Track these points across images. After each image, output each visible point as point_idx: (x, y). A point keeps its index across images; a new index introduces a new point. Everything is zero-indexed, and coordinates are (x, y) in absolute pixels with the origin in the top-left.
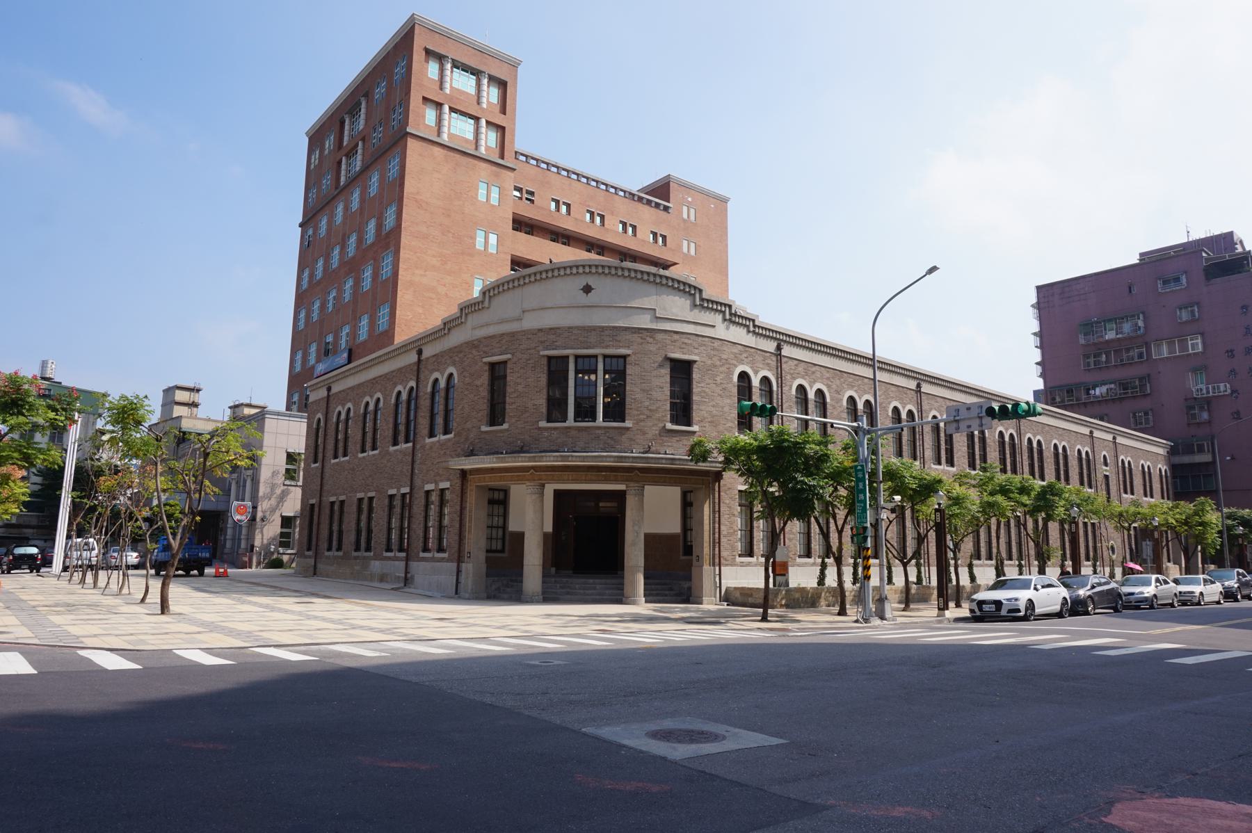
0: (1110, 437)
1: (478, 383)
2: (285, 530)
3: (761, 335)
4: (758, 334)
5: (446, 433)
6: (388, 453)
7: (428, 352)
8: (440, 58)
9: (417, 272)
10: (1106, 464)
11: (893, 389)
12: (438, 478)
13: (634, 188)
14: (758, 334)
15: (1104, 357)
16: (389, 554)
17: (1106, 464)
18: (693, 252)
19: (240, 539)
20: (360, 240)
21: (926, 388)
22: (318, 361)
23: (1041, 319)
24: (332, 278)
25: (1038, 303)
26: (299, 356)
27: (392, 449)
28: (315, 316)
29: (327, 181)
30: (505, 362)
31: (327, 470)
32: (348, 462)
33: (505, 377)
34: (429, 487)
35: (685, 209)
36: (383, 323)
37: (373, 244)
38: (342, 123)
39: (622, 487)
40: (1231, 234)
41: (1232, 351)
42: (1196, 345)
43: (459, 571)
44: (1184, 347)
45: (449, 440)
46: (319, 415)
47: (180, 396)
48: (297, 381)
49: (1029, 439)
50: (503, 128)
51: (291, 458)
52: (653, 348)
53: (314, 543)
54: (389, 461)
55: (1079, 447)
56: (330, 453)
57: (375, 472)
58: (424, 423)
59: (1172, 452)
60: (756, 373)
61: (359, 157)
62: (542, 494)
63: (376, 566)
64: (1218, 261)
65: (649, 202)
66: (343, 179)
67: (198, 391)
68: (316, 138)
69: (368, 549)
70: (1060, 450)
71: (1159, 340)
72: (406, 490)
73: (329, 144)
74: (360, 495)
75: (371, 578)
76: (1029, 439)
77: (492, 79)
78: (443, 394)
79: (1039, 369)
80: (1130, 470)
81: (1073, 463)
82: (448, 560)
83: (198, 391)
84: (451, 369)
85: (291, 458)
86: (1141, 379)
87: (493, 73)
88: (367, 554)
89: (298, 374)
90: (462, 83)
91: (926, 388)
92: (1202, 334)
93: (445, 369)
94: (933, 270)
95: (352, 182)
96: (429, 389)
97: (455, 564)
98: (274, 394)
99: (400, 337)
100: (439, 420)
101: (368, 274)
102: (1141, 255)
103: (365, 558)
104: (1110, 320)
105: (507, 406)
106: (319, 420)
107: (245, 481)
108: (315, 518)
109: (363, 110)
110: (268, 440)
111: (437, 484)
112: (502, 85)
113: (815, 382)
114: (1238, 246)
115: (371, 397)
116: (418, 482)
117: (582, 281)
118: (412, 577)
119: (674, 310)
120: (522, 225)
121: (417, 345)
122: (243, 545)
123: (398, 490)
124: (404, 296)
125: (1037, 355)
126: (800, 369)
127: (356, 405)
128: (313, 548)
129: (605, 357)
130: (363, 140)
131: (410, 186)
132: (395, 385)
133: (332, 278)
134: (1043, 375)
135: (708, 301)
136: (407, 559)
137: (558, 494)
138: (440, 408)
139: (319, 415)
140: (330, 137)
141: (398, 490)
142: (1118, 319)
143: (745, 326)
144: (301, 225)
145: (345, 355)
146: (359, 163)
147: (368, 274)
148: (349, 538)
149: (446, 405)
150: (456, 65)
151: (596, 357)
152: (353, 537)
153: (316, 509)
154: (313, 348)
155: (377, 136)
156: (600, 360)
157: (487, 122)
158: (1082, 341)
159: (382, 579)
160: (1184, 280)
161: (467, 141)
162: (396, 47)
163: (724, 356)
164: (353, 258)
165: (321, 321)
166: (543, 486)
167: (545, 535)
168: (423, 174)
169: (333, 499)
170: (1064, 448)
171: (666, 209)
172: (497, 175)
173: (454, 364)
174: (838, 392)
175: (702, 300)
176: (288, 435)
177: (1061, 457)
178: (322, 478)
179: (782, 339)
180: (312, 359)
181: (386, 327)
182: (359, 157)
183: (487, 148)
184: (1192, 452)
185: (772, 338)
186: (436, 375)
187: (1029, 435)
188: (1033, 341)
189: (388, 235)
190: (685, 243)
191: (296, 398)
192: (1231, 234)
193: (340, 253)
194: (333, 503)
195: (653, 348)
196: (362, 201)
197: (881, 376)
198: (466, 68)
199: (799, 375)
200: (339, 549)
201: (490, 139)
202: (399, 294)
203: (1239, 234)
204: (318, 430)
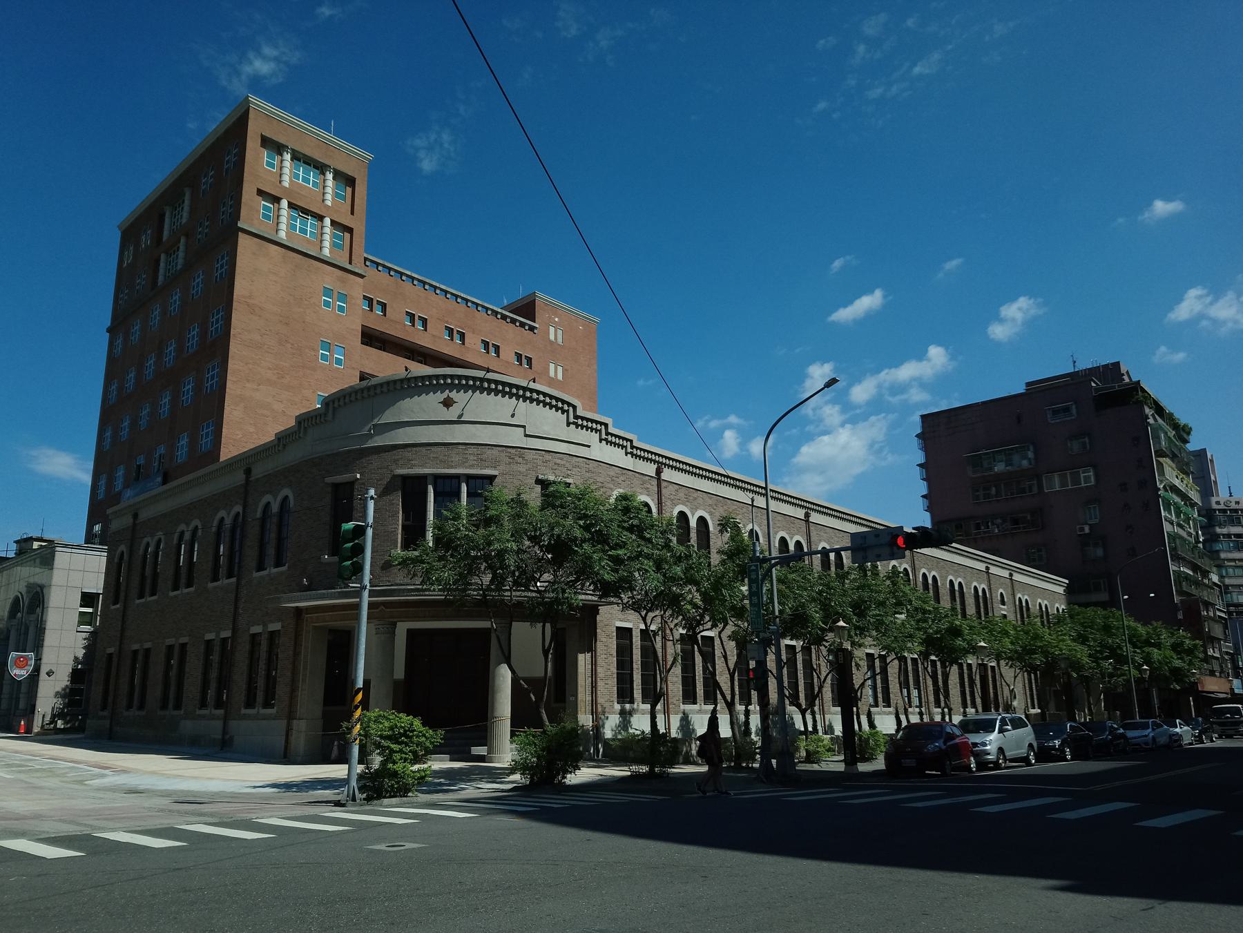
0: (1006, 574)
2: (77, 686)
3: (640, 457)
4: (636, 456)
5: (278, 565)
9: (247, 385)
10: (1003, 603)
14: (636, 456)
15: (993, 490)
17: (1003, 603)
18: (560, 377)
19: (18, 699)
21: (815, 518)
22: (126, 486)
23: (926, 448)
26: (103, 482)
27: (211, 585)
28: (125, 434)
34: (256, 629)
36: (205, 443)
38: (162, 216)
40: (1117, 365)
43: (289, 731)
44: (1076, 481)
48: (97, 511)
49: (924, 575)
52: (522, 468)
55: (975, 584)
58: (251, 554)
59: (1069, 590)
61: (181, 254)
62: (393, 634)
65: (513, 321)
66: (161, 278)
68: (129, 234)
72: (226, 634)
73: (146, 240)
74: (170, 641)
76: (924, 575)
78: (275, 520)
81: (970, 601)
82: (275, 718)
84: (286, 492)
85: (88, 599)
87: (340, 168)
88: (176, 713)
91: (815, 518)
92: (1095, 467)
96: (259, 514)
98: (70, 522)
99: (227, 452)
100: (271, 551)
102: (1028, 384)
107: (27, 628)
108: (114, 670)
109: (187, 202)
111: (265, 625)
113: (697, 509)
114: (1126, 377)
115: (188, 524)
117: (441, 396)
118: (231, 738)
119: (546, 428)
120: (371, 338)
121: (247, 461)
122: (22, 705)
123: (218, 634)
124: (232, 413)
125: (923, 488)
126: (681, 495)
130: (187, 236)
131: (241, 287)
134: (929, 509)
136: (226, 719)
137: (411, 633)
138: (272, 536)
139: (122, 548)
140: (144, 234)
141: (218, 634)
143: (623, 447)
144: (109, 330)
146: (180, 261)
148: (154, 693)
149: (279, 532)
151: (457, 477)
153: (115, 659)
154: (120, 473)
157: (333, 223)
162: (227, 132)
166: (395, 624)
167: (396, 683)
169: (135, 647)
170: (960, 584)
171: (532, 329)
175: (576, 417)
176: (81, 571)
178: (123, 622)
180: (119, 485)
182: (181, 254)
185: (651, 460)
186: (268, 498)
187: (923, 570)
190: (552, 366)
191: (97, 528)
192: (1117, 365)
194: (135, 652)
195: (522, 468)
197: (774, 506)
199: (680, 502)
200: (141, 707)
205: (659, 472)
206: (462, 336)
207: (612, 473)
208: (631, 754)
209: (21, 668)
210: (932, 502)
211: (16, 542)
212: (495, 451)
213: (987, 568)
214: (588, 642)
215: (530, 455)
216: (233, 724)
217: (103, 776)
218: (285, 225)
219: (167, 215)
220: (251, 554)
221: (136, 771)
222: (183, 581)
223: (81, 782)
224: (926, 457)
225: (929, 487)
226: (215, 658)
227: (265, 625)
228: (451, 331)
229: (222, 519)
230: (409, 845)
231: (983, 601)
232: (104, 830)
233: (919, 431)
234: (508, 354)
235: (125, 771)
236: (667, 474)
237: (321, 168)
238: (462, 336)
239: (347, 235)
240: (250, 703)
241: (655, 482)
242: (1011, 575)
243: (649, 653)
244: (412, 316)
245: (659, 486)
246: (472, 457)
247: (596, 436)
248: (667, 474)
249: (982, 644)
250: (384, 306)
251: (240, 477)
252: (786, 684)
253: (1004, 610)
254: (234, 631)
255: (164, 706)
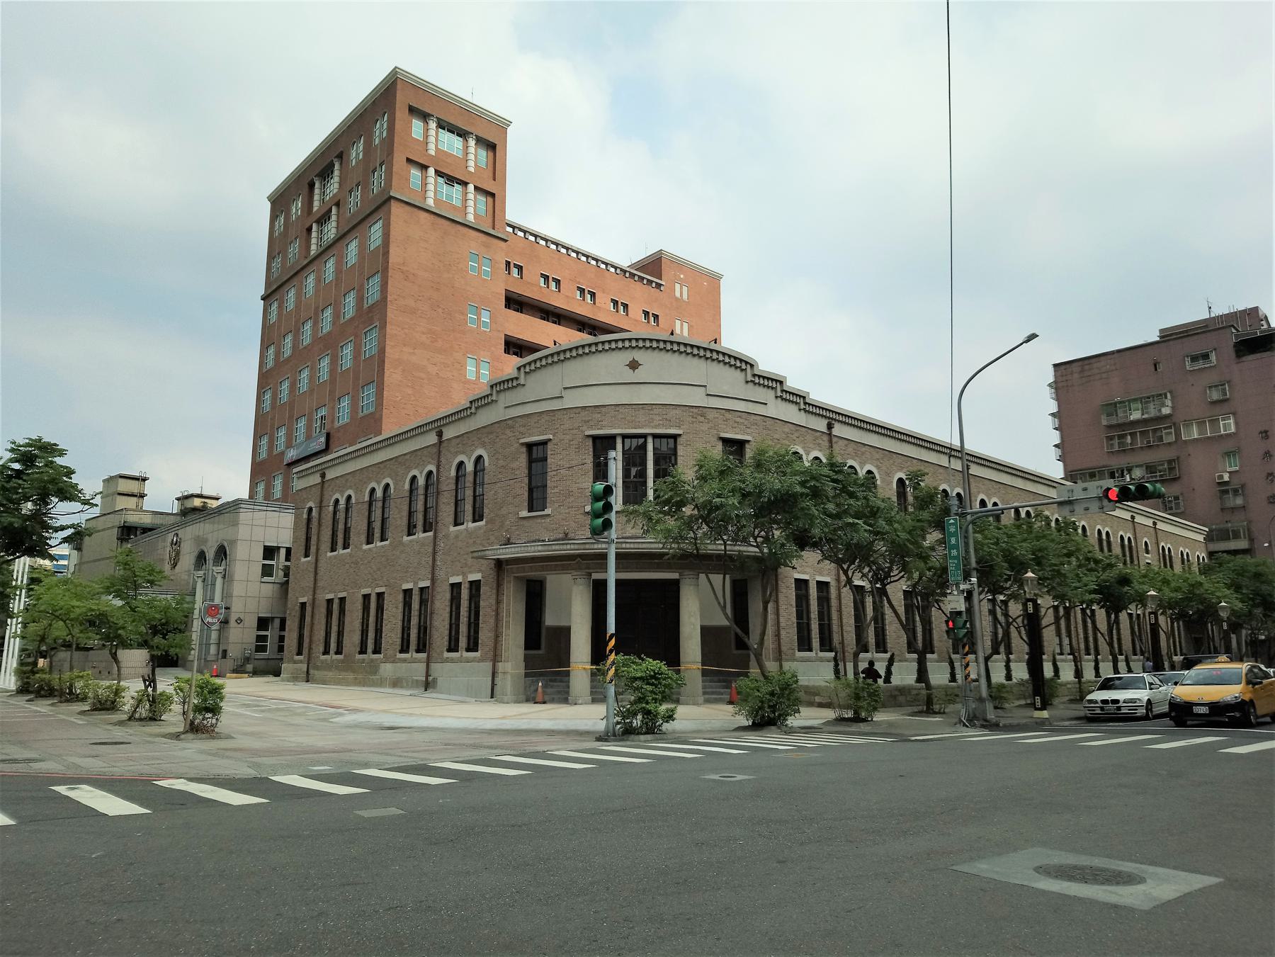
0: (1149, 522)
1: (515, 465)
6: (401, 543)
7: (449, 433)
8: (425, 117)
9: (405, 349)
10: (1147, 552)
11: (941, 470)
12: (466, 569)
13: (625, 264)
15: (1129, 439)
16: (403, 656)
17: (1147, 552)
19: (208, 645)
20: (336, 315)
23: (1058, 399)
24: (303, 356)
25: (1055, 382)
29: (294, 250)
30: (544, 443)
31: (322, 564)
32: (350, 555)
33: (546, 459)
35: (678, 286)
37: (352, 319)
39: (675, 576)
41: (1266, 432)
42: (1228, 425)
45: (480, 528)
46: (311, 504)
47: (124, 486)
50: (493, 195)
51: (270, 552)
52: (705, 427)
53: (306, 645)
54: (402, 552)
56: (326, 544)
57: (352, 572)
59: (1209, 538)
60: (808, 454)
63: (387, 669)
64: (1253, 339)
66: (313, 247)
67: (144, 480)
68: (280, 201)
69: (377, 650)
70: (1104, 537)
71: (1188, 424)
72: (426, 583)
73: (297, 207)
74: (365, 591)
75: (380, 683)
77: (480, 141)
79: (1059, 452)
80: (1170, 557)
82: (481, 660)
83: (144, 480)
86: (1170, 462)
89: (263, 462)
90: (451, 143)
91: (974, 470)
92: (1234, 414)
93: (473, 451)
94: (1033, 336)
95: (325, 251)
96: (453, 473)
97: (489, 665)
101: (348, 351)
102: (1161, 331)
103: (372, 660)
104: (1135, 400)
105: (549, 490)
106: (310, 509)
107: (214, 579)
110: (243, 532)
111: (464, 575)
112: (491, 147)
115: (379, 483)
116: (440, 574)
117: (628, 356)
118: (435, 680)
120: (515, 302)
123: (416, 583)
125: (1056, 438)
127: (359, 491)
128: (305, 651)
129: (655, 436)
130: (338, 204)
132: (409, 469)
133: (303, 356)
135: (759, 376)
140: (299, 198)
141: (416, 583)
142: (1145, 400)
144: (263, 298)
145: (323, 439)
147: (348, 351)
150: (441, 125)
151: (644, 436)
152: (357, 638)
153: (309, 609)
155: (355, 201)
156: (650, 440)
157: (476, 188)
158: (1104, 423)
159: (396, 683)
160: (1213, 357)
161: (454, 207)
163: (776, 436)
164: (329, 333)
165: (291, 403)
168: (409, 240)
171: (659, 286)
172: (487, 246)
173: (483, 445)
174: (888, 474)
177: (1105, 543)
178: (316, 573)
179: (833, 417)
181: (372, 410)
183: (476, 216)
184: (1228, 539)
185: (822, 416)
188: (1050, 423)
189: (371, 308)
192: (1256, 309)
193: (280, 307)
194: (330, 602)
196: (338, 271)
198: (452, 129)
201: (475, 208)
202: (387, 373)
203: (1264, 310)
204: (309, 520)
205: (830, 427)
206: (593, 295)
207: (787, 430)
208: (817, 699)
209: (213, 617)
210: (1065, 450)
211: (178, 499)
212: (678, 411)
213: (1133, 517)
214: (771, 594)
215: (711, 415)
216: (433, 666)
217: (341, 715)
218: (435, 192)
219: (317, 185)
220: (446, 511)
221: (369, 711)
222: (377, 535)
223: (325, 720)
224: (1059, 406)
225: (1062, 438)
226: (415, 605)
227: (464, 575)
228: (582, 291)
229: (414, 478)
230: (739, 777)
231: (1129, 549)
232: (367, 765)
233: (1052, 379)
234: (636, 312)
235: (356, 710)
236: (838, 430)
237: (463, 134)
238: (593, 295)
239: (490, 199)
240: (453, 647)
241: (826, 438)
242: (1155, 524)
243: (824, 600)
244: (546, 278)
245: (830, 441)
246: (657, 418)
247: (771, 393)
248: (838, 430)
249: (1152, 593)
250: (520, 268)
251: (432, 439)
252: (611, 628)
253: (1149, 558)
254: (433, 580)
255: (363, 651)
